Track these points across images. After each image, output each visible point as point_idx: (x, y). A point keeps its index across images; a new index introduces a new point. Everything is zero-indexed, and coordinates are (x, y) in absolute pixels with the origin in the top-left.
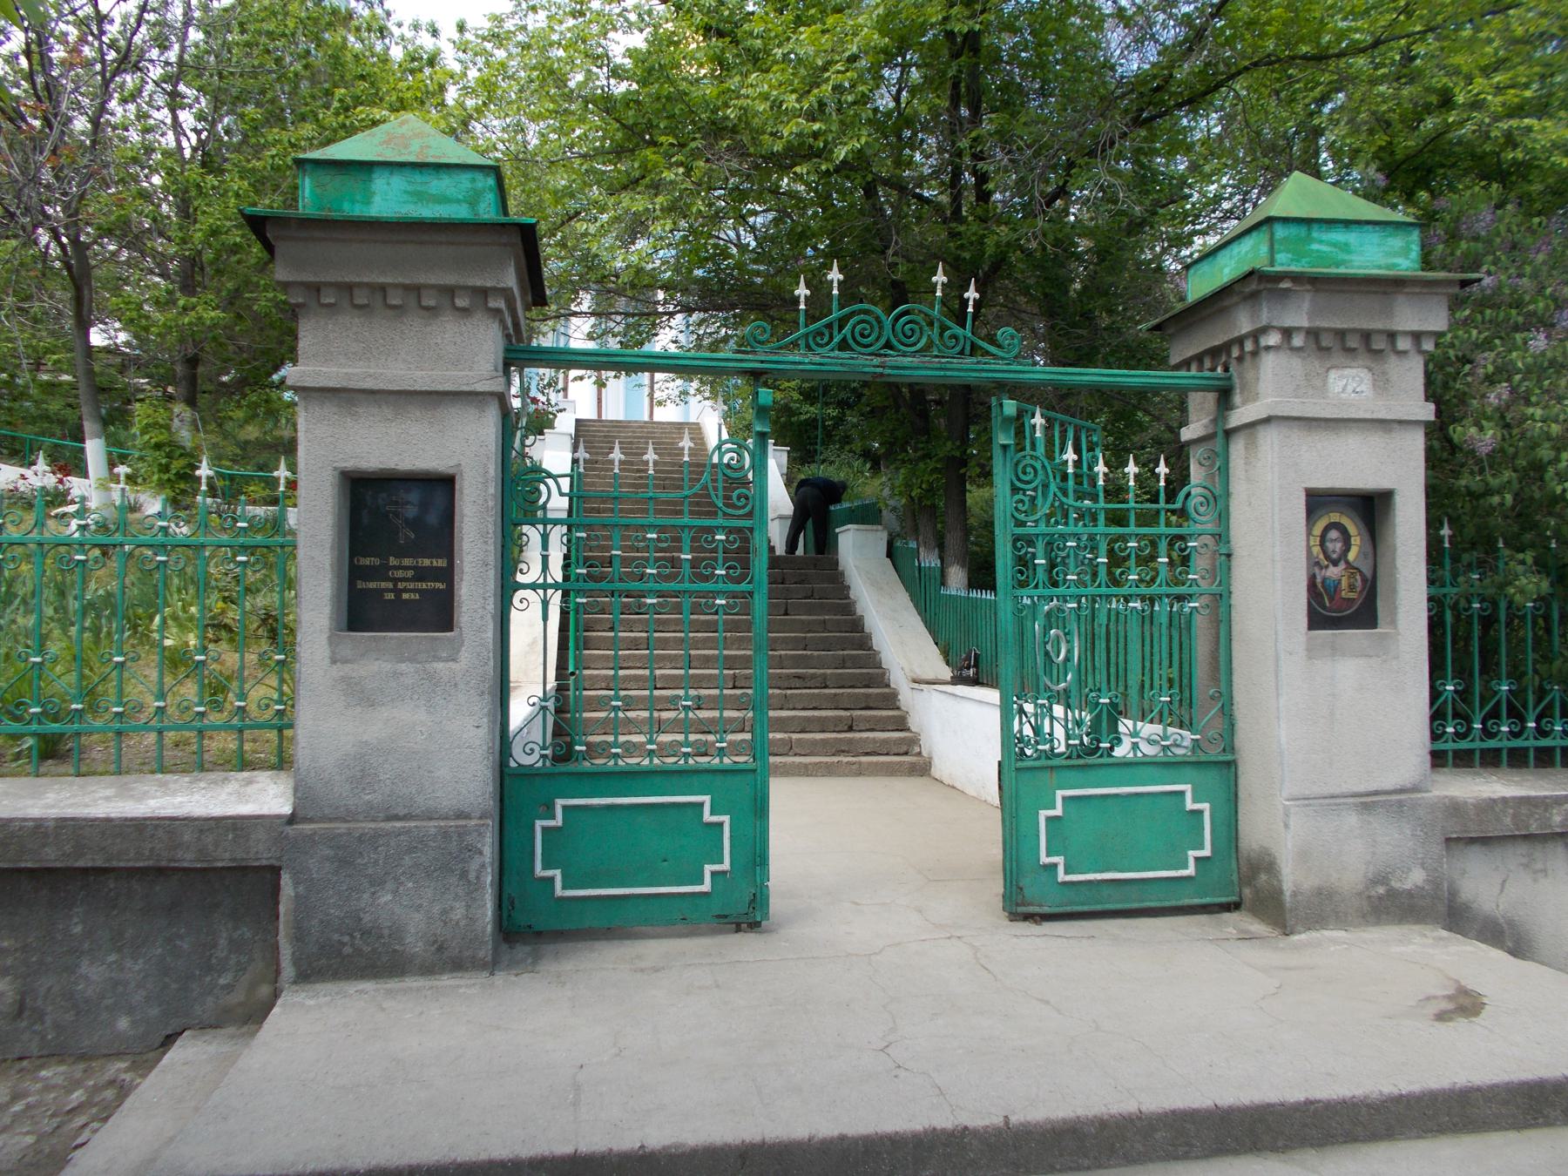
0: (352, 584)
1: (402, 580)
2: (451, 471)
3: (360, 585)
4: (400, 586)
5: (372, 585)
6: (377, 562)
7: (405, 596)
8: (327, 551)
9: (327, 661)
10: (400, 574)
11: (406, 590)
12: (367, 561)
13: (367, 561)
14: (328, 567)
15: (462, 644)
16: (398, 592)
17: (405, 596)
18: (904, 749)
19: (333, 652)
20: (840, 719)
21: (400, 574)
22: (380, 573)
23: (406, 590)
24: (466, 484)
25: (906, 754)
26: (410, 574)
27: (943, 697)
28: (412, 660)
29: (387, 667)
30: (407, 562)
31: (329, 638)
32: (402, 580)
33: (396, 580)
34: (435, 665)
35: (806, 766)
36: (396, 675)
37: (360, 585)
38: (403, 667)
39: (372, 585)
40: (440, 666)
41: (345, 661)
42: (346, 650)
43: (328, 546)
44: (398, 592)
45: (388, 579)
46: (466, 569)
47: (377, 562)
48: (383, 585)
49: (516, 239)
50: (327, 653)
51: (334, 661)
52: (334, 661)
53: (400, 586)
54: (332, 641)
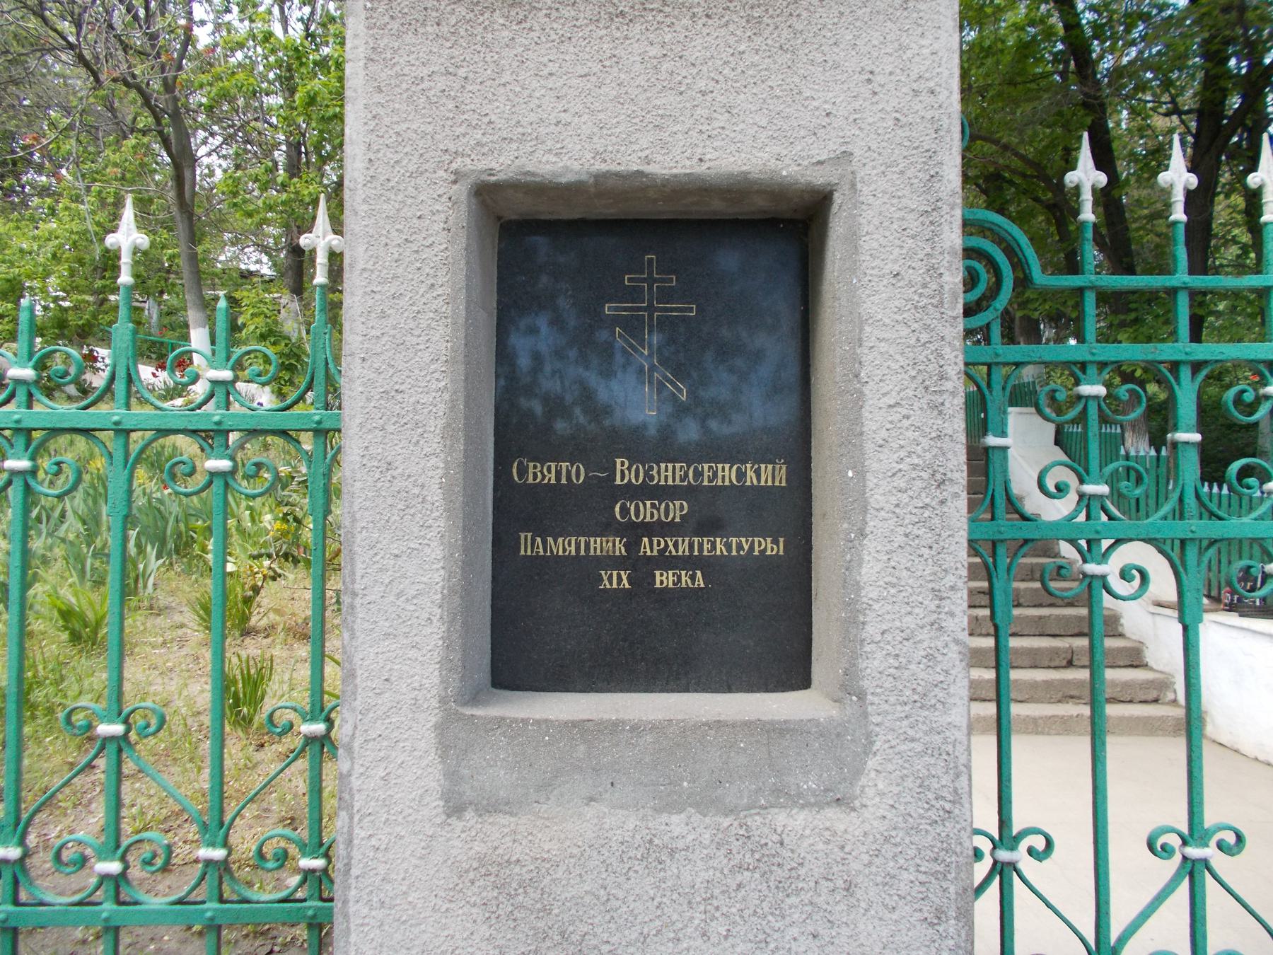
0: (503, 544)
1: (652, 529)
2: (819, 178)
3: (529, 545)
4: (649, 547)
5: (564, 546)
6: (577, 473)
7: (665, 579)
8: (434, 443)
9: (435, 804)
10: (646, 511)
11: (666, 561)
12: (546, 473)
13: (546, 473)
14: (435, 495)
15: (868, 750)
16: (642, 568)
17: (665, 579)
18: (1152, 695)
19: (452, 776)
20: (1055, 652)
21: (646, 511)
22: (592, 506)
23: (666, 561)
24: (868, 219)
25: (1156, 701)
26: (677, 510)
27: (1223, 630)
28: (707, 803)
29: (623, 823)
30: (667, 473)
31: (441, 729)
32: (652, 529)
33: (634, 532)
34: (780, 818)
35: (1035, 720)
36: (656, 853)
37: (529, 545)
38: (677, 823)
39: (564, 546)
40: (793, 821)
41: (490, 807)
42: (493, 771)
43: (435, 425)
44: (642, 568)
45: (608, 528)
46: (877, 498)
47: (577, 473)
48: (600, 545)
49: (10, 936)
50: (433, 779)
51: (455, 808)
52: (455, 808)
53: (649, 547)
54: (452, 741)
